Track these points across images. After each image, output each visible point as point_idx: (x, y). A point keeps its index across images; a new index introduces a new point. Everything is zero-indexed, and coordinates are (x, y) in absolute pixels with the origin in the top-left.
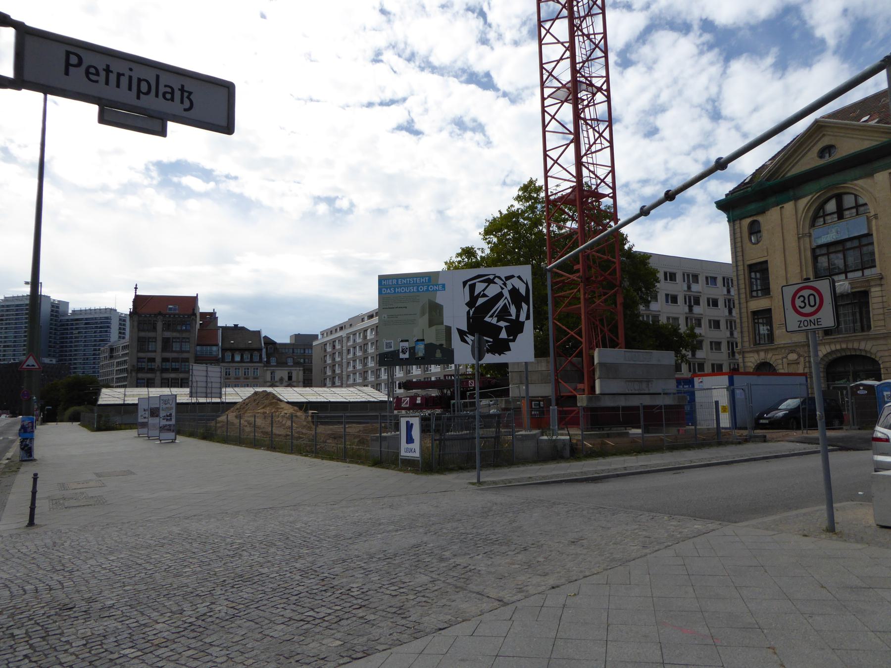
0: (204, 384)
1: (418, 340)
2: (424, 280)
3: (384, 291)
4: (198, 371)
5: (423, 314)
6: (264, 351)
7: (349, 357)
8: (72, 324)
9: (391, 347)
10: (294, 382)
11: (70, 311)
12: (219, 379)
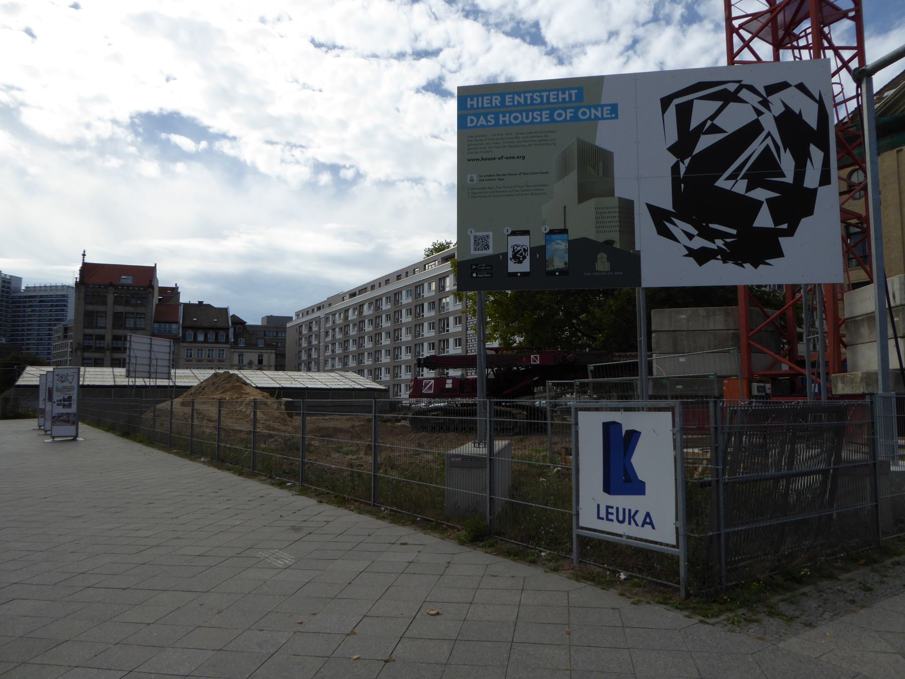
0: (147, 362)
1: (552, 232)
2: (567, 96)
3: (472, 121)
4: (139, 344)
5: (564, 171)
6: (231, 330)
7: (327, 340)
8: (25, 302)
9: (487, 247)
10: (265, 366)
11: (23, 288)
12: (168, 355)
